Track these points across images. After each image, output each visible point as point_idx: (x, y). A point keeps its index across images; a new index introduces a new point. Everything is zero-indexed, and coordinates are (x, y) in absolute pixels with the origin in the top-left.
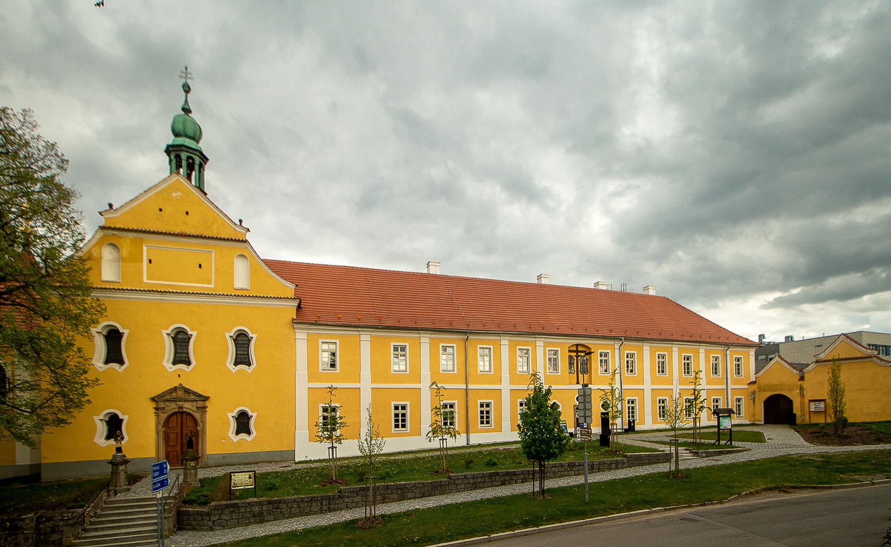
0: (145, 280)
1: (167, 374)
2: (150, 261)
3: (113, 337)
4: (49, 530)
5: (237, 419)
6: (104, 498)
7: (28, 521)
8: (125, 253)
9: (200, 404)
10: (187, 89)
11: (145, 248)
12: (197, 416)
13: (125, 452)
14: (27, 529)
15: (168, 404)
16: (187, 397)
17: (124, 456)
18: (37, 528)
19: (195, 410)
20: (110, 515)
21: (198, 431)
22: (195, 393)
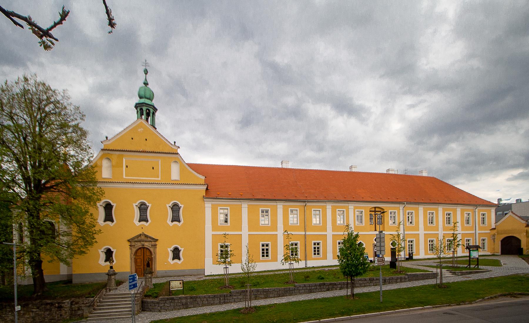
0: (124, 177)
1: (137, 227)
2: (127, 167)
3: (108, 207)
4: (77, 309)
6: (104, 293)
7: (66, 304)
9: (153, 243)
11: (124, 160)
12: (152, 250)
14: (66, 308)
15: (136, 243)
16: (146, 239)
18: (71, 307)
22: (150, 238)
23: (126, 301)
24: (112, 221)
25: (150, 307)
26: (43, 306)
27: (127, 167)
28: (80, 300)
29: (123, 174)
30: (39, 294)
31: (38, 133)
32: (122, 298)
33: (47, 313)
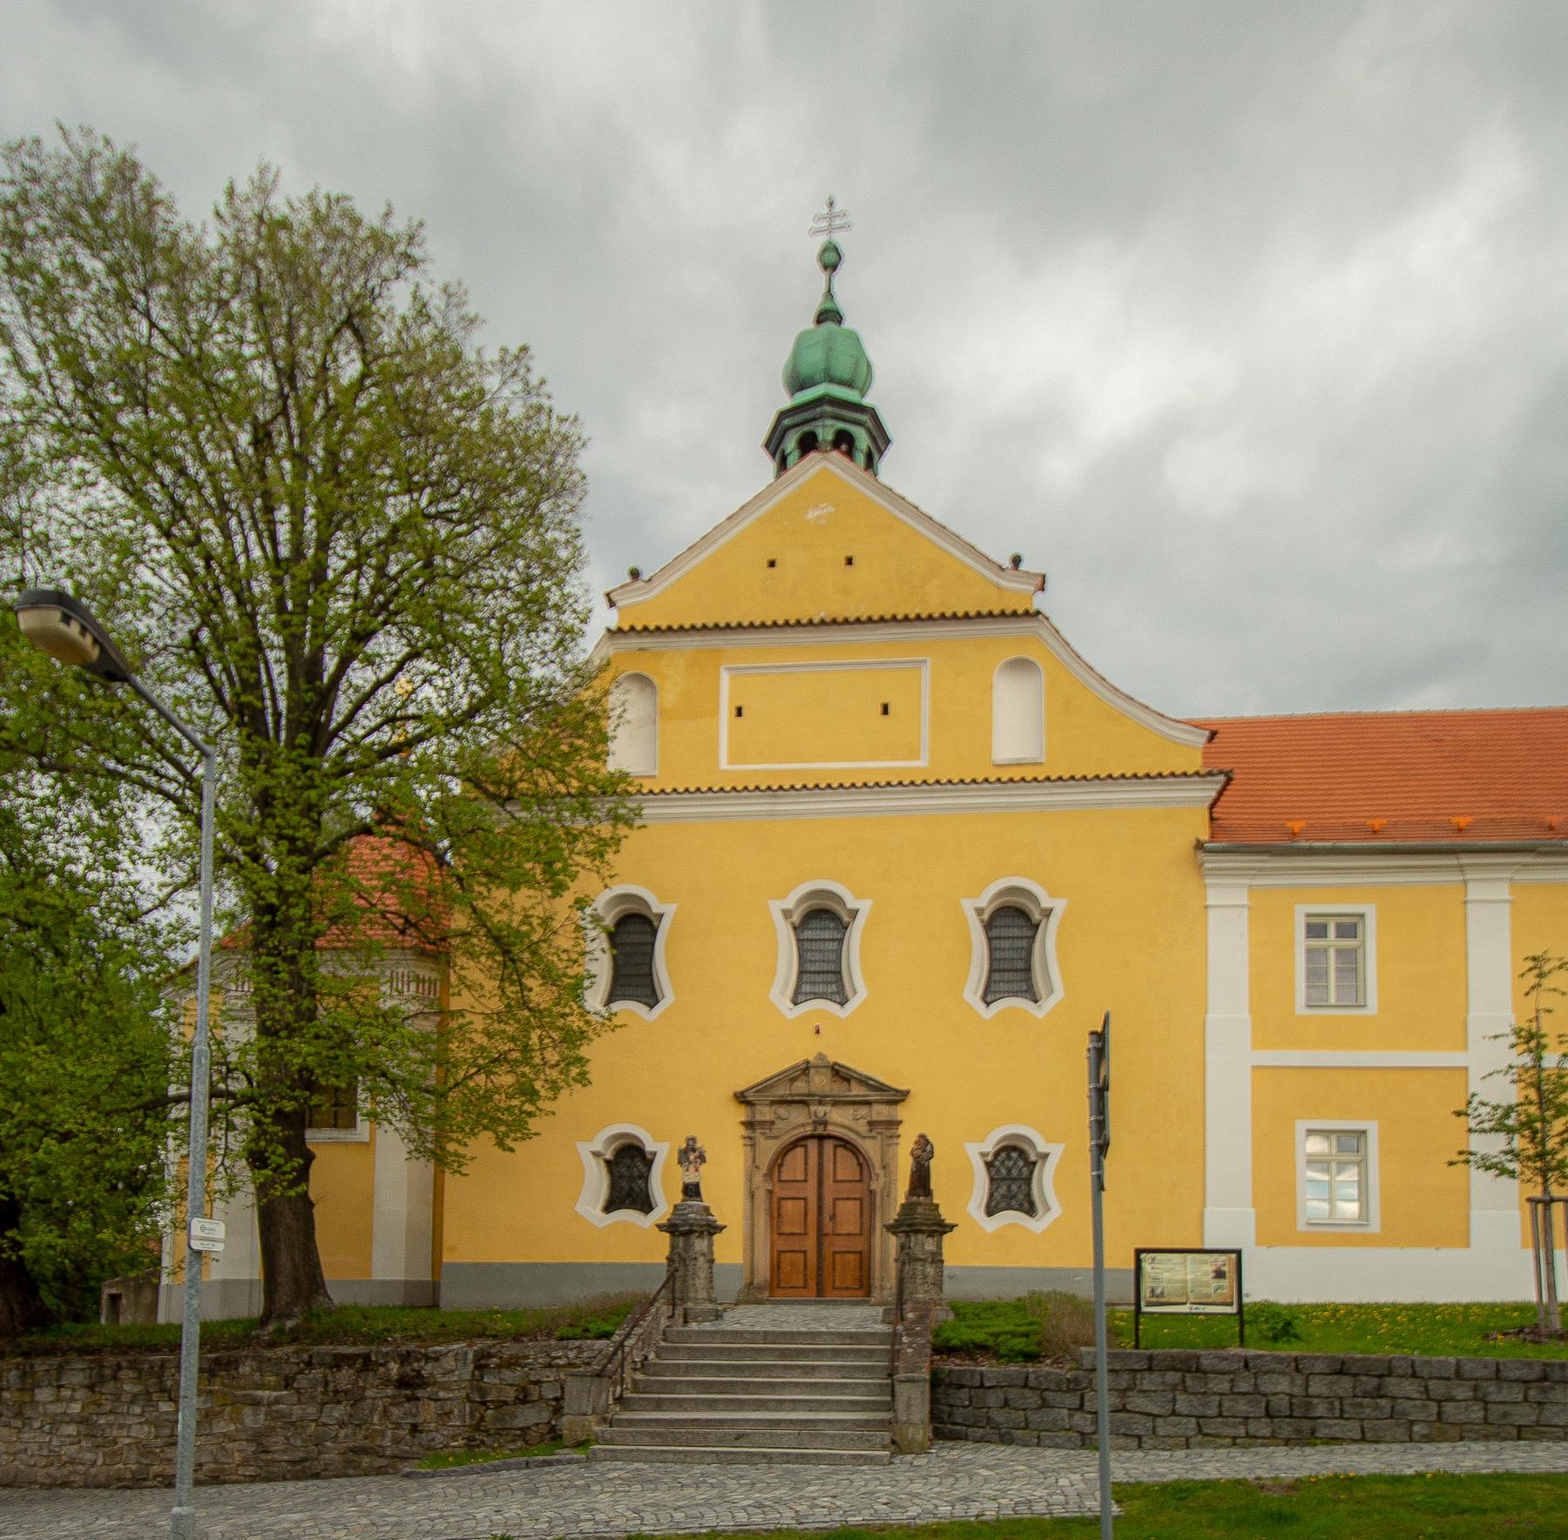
1: (778, 1029)
2: (739, 712)
3: (634, 933)
4: (510, 1394)
5: (989, 1165)
6: (664, 1322)
7: (449, 1362)
8: (670, 694)
9: (881, 1112)
10: (831, 261)
11: (725, 677)
12: (870, 1147)
13: (708, 1197)
14: (446, 1387)
15: (782, 1111)
16: (838, 1089)
17: (707, 1209)
18: (477, 1385)
19: (864, 1129)
20: (689, 1369)
22: (865, 1081)
23: (812, 1370)
24: (652, 999)
25: (999, 1416)
26: (317, 1373)
27: (739, 712)
28: (531, 1349)
29: (714, 752)
30: (289, 1324)
31: (327, 443)
32: (783, 1354)
33: (339, 1411)
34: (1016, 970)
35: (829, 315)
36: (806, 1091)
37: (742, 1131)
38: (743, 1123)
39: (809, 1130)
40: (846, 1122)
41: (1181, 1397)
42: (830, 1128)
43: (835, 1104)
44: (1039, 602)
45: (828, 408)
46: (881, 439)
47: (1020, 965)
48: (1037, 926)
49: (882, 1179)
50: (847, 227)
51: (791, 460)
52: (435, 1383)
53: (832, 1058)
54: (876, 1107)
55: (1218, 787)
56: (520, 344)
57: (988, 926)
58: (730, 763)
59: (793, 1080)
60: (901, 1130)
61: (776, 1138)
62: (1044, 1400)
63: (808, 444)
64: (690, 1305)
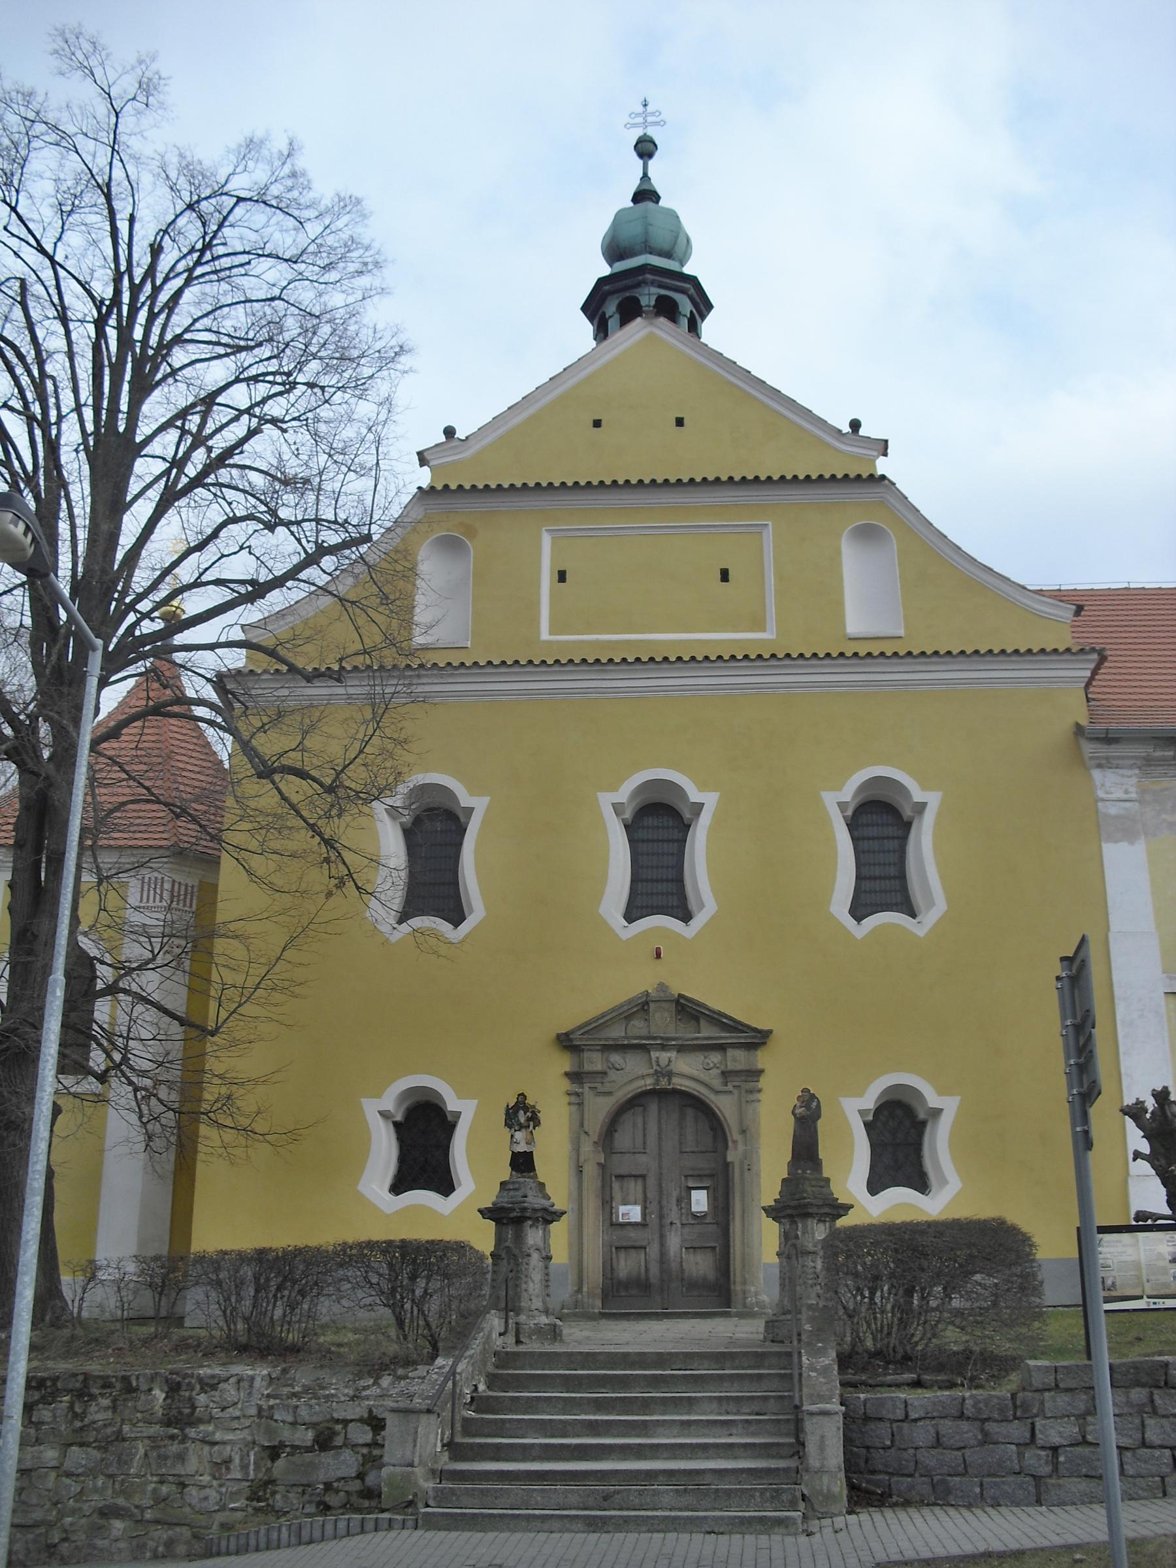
0: (545, 635)
1: (621, 957)
2: (562, 576)
7: (230, 1391)
10: (645, 149)
11: (546, 541)
12: (725, 1106)
15: (616, 1058)
16: (686, 1032)
19: (717, 1083)
21: (727, 1166)
34: (890, 878)
35: (645, 195)
36: (644, 1032)
37: (566, 1084)
38: (567, 1074)
39: (648, 1083)
40: (695, 1073)
41: (1150, 1422)
42: (675, 1080)
43: (681, 1049)
44: (882, 466)
45: (649, 277)
46: (703, 305)
47: (892, 871)
48: (908, 825)
49: (741, 1147)
50: (661, 123)
51: (613, 323)
52: (211, 1419)
53: (678, 987)
54: (730, 1053)
55: (1092, 666)
56: (236, 138)
57: (853, 825)
58: (551, 634)
59: (629, 1018)
60: (763, 1082)
61: (610, 1093)
62: (986, 1434)
63: (630, 311)
64: (522, 1318)
